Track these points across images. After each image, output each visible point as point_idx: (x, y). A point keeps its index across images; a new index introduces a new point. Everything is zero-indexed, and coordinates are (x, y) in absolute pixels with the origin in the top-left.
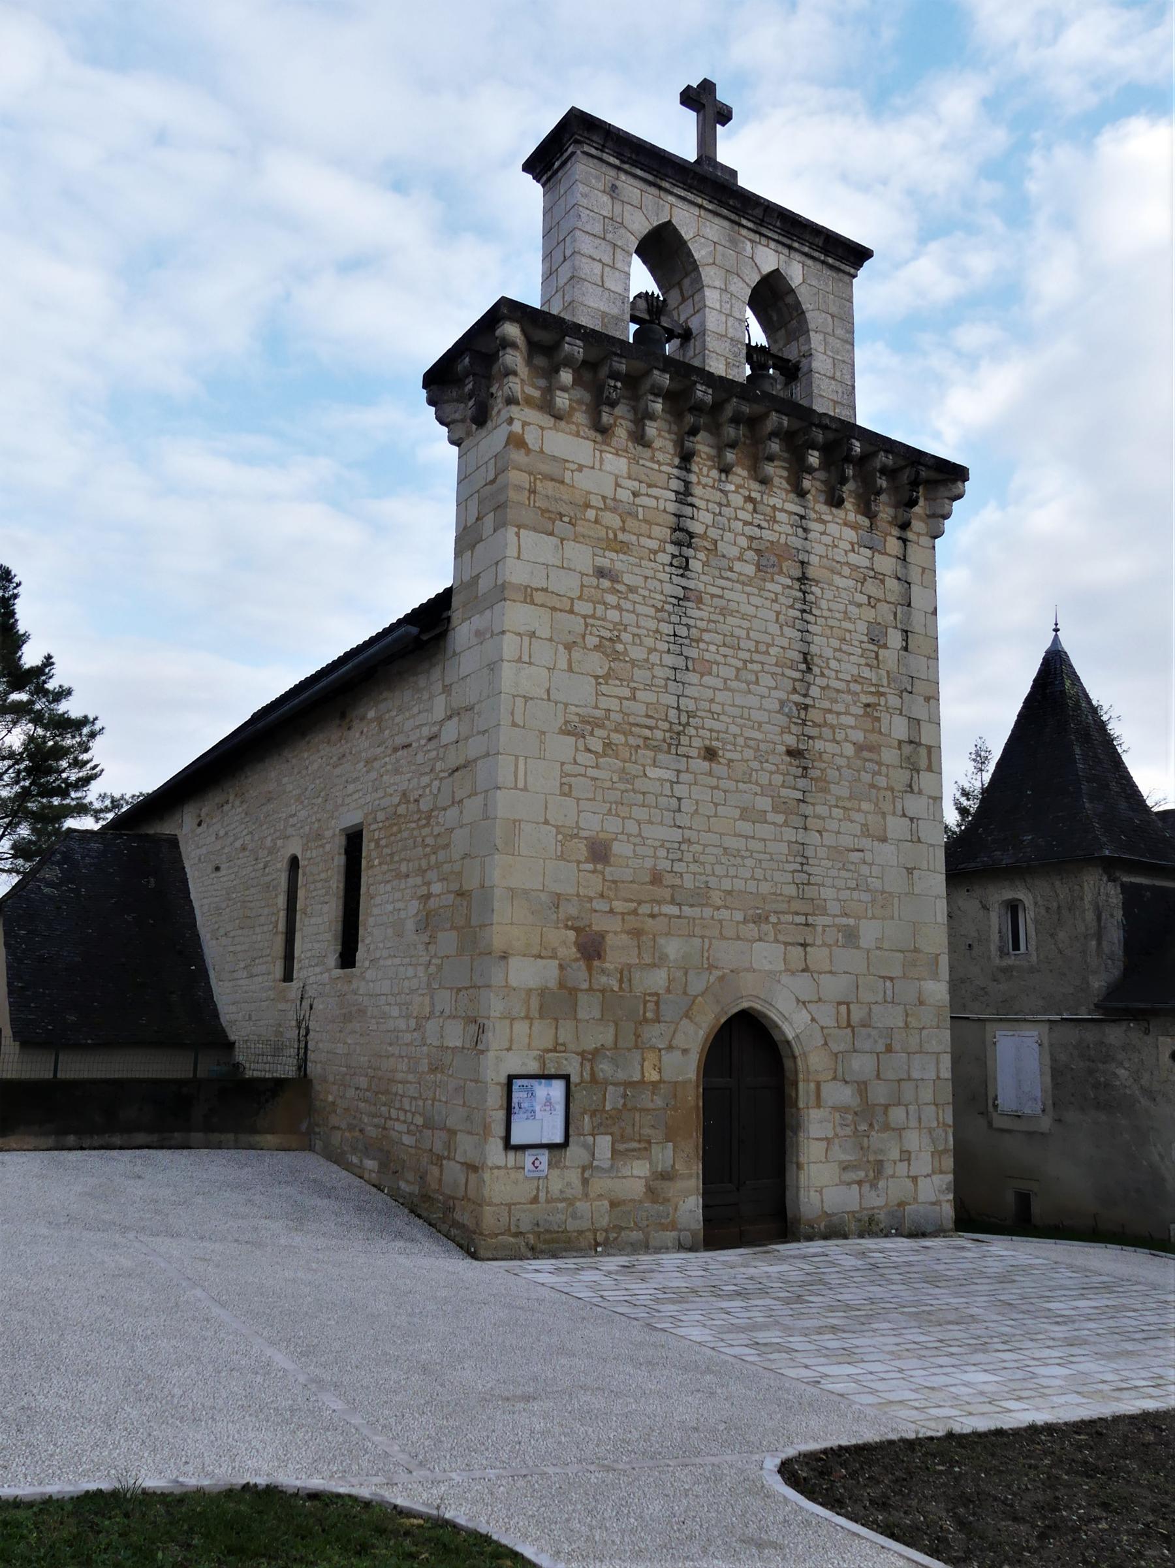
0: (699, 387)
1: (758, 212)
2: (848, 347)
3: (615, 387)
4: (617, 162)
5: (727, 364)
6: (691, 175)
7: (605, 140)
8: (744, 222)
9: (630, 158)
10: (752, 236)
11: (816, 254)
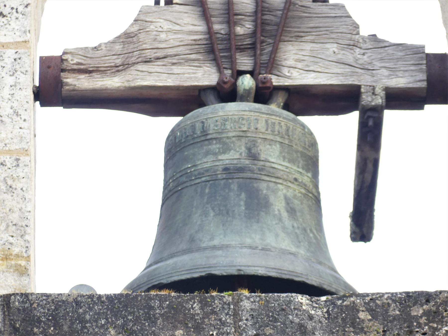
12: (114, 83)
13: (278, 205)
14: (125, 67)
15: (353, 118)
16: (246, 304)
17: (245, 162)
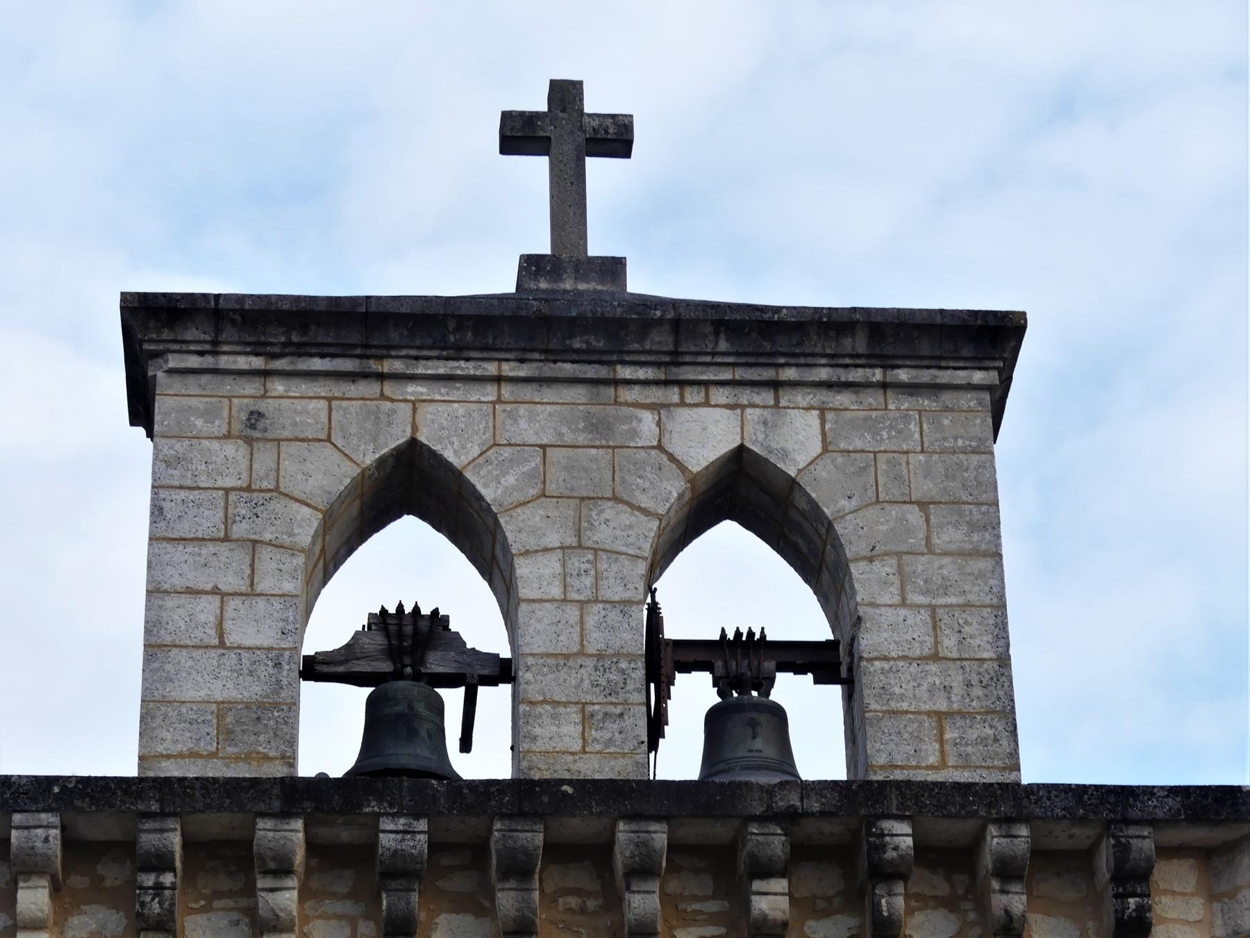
0: (386, 824)
1: (661, 340)
2: (985, 564)
3: (159, 887)
4: (257, 363)
5: (587, 719)
6: (451, 325)
7: (218, 331)
8: (625, 372)
9: (284, 345)
10: (656, 395)
11: (856, 375)
12: (341, 669)
13: (423, 733)
14: (346, 661)
15: (461, 691)
16: (406, 784)
17: (293, 363)
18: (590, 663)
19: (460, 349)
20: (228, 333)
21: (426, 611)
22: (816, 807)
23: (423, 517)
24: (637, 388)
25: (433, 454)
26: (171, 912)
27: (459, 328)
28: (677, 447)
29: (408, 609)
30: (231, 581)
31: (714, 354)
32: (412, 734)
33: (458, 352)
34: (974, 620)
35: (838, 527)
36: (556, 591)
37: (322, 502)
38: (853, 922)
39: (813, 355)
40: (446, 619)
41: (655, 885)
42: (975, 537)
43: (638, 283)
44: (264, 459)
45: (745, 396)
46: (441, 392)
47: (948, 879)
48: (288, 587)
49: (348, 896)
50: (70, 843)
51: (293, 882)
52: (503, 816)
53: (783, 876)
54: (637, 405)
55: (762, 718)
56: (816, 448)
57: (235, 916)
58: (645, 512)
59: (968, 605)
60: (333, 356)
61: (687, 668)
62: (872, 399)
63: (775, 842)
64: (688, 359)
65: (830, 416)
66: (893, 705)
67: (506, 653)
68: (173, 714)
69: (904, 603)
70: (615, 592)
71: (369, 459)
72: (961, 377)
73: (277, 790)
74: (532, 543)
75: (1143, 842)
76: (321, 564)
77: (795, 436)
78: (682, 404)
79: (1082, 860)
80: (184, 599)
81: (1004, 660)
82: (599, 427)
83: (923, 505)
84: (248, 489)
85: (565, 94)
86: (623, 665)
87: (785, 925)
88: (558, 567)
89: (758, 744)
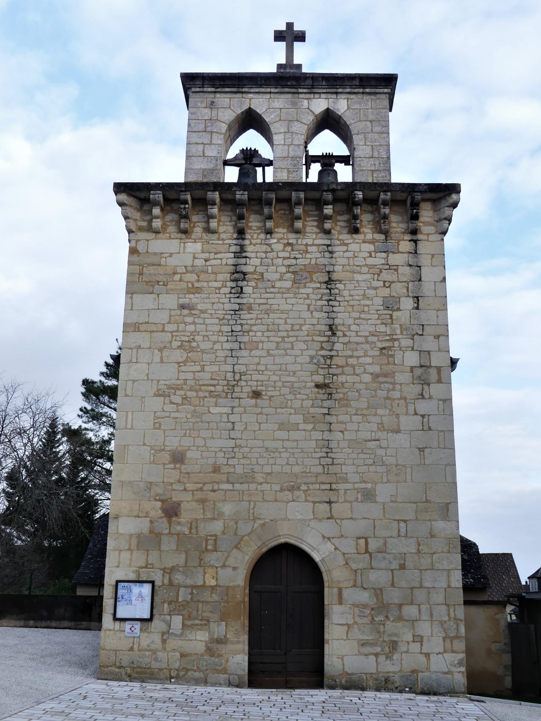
0: (238, 193)
1: (309, 82)
2: (385, 135)
3: (185, 208)
4: (213, 90)
5: (289, 172)
7: (203, 81)
9: (219, 85)
10: (308, 96)
11: (356, 90)
12: (233, 163)
14: (234, 161)
15: (261, 168)
18: (290, 159)
19: (261, 85)
20: (206, 82)
21: (253, 149)
22: (340, 188)
23: (255, 129)
24: (303, 94)
25: (255, 111)
26: (188, 213)
27: (260, 80)
28: (312, 108)
29: (249, 149)
30: (206, 141)
31: (322, 85)
32: (248, 177)
33: (261, 86)
34: (382, 149)
35: (350, 127)
36: (283, 142)
37: (228, 122)
38: (349, 216)
39: (346, 85)
40: (258, 151)
41: (301, 207)
42: (383, 129)
43: (304, 70)
44: (214, 112)
45: (329, 96)
46: (257, 96)
47: (372, 207)
48: (220, 142)
49: (230, 211)
50: (166, 199)
51: (216, 207)
52: (265, 191)
53: (331, 204)
54: (303, 98)
55: (331, 172)
56: (346, 108)
57: (204, 216)
58: (304, 124)
59: (381, 145)
60: (231, 88)
61: (314, 162)
62: (360, 96)
63: (329, 196)
64: (316, 87)
65: (349, 100)
66: (362, 168)
67: (272, 159)
68: (192, 172)
69: (365, 145)
70: (296, 142)
71: (239, 112)
72: (381, 90)
73: (212, 185)
74: (277, 131)
75: (418, 197)
76: (229, 139)
77: (341, 105)
78: (314, 98)
79: (404, 202)
80: (195, 145)
81: (389, 158)
82: (294, 104)
83: (371, 121)
84: (211, 120)
85: (290, 25)
86: (298, 159)
87: (332, 216)
88: (283, 137)
89: (330, 178)
